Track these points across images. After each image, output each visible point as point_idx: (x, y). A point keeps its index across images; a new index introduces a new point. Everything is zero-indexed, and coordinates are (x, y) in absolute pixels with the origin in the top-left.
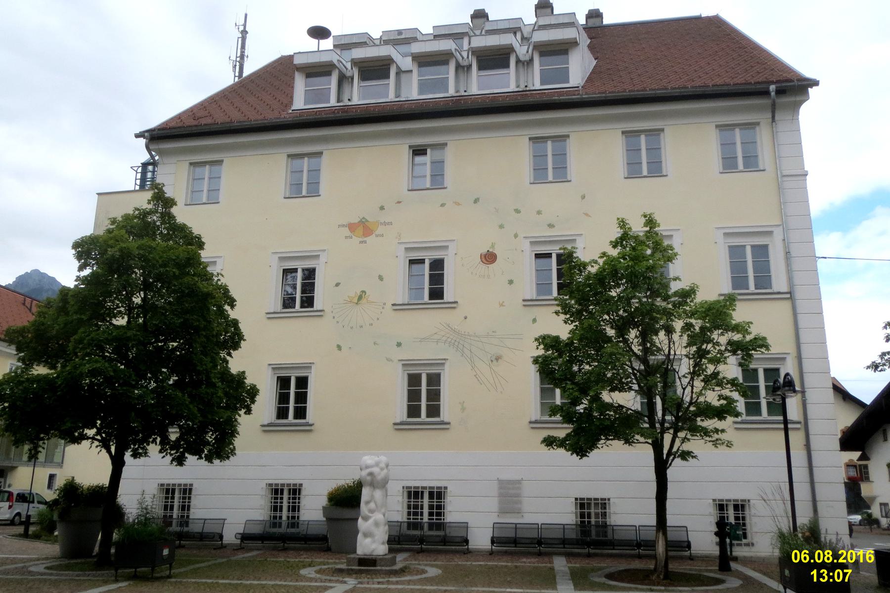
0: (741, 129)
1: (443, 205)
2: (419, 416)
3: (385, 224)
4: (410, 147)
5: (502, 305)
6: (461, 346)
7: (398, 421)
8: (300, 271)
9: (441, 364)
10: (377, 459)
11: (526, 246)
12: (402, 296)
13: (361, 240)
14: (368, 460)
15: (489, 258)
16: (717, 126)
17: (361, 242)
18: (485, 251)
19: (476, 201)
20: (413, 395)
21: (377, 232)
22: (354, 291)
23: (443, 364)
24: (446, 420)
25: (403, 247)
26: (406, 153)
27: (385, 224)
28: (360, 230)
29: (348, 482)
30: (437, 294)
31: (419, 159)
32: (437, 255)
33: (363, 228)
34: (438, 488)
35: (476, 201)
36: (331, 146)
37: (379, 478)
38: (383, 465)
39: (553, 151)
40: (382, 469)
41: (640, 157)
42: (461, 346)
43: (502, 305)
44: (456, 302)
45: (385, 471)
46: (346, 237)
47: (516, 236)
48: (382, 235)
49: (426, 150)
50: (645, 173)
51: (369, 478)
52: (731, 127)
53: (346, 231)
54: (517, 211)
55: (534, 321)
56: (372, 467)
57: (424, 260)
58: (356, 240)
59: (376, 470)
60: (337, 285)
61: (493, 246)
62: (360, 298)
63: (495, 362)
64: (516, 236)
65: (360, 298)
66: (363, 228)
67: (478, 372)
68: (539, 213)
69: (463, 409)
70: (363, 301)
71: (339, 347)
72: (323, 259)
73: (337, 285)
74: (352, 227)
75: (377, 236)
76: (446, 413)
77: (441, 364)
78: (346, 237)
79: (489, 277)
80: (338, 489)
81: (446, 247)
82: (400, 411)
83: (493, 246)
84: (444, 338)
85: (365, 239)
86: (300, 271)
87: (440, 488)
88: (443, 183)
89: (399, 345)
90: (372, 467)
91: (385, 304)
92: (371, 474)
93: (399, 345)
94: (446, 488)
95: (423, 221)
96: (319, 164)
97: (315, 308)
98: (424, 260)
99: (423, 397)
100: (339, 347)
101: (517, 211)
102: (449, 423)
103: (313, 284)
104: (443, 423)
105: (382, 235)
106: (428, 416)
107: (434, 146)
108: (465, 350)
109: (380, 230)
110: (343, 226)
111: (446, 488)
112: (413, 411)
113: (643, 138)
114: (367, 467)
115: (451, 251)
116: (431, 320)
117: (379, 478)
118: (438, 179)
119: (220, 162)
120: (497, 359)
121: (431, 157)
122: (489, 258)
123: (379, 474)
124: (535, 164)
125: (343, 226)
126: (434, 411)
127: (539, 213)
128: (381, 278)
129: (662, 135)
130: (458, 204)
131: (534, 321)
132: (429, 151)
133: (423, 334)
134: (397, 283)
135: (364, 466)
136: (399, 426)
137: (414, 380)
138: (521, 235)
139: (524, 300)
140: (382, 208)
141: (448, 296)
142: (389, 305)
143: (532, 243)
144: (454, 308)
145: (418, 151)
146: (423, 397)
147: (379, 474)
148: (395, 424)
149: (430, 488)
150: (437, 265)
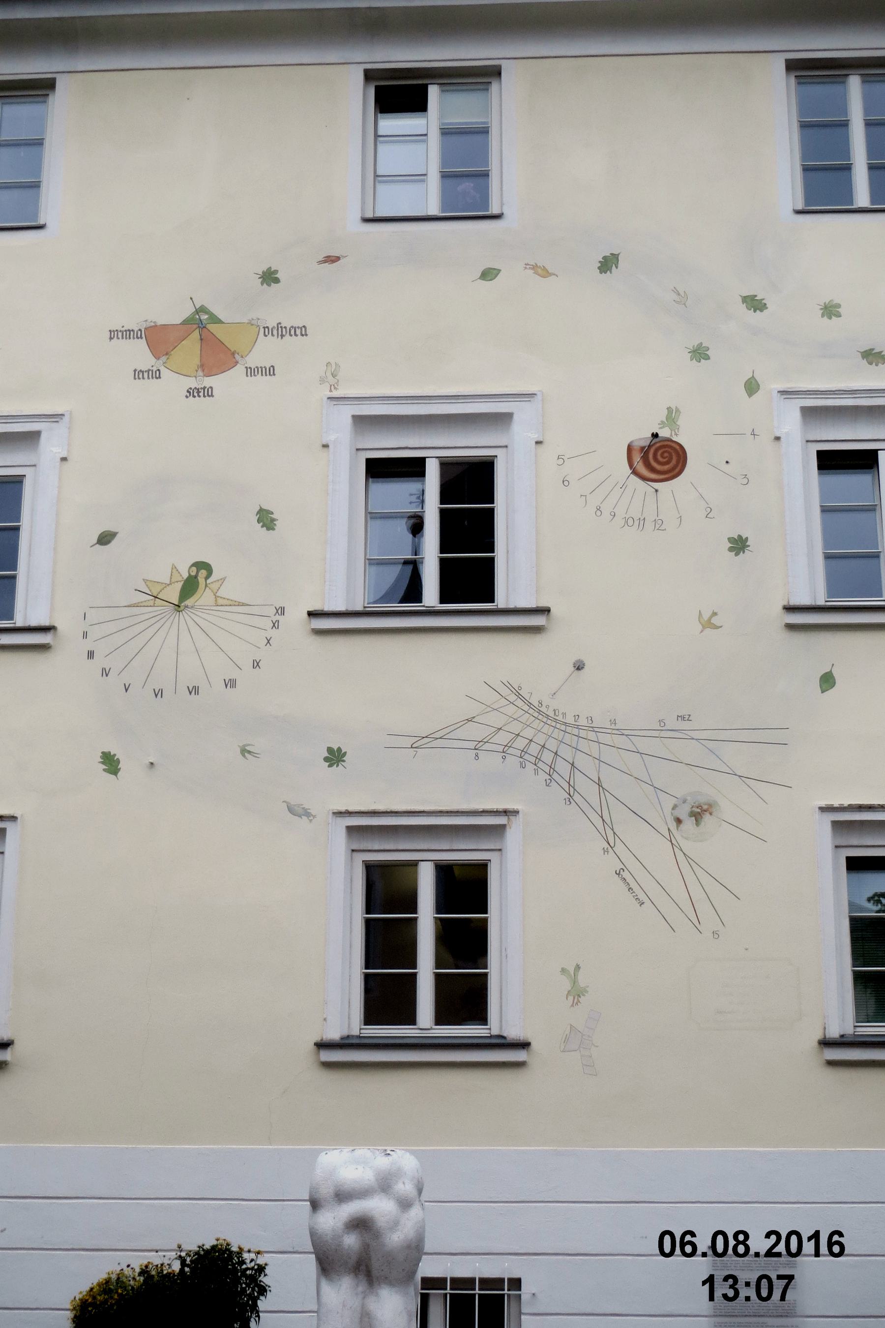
0: (866, 80)
1: (488, 274)
2: (410, 1018)
3: (281, 331)
4: (369, 76)
5: (709, 624)
6: (563, 768)
7: (334, 1035)
8: (433, 471)
9: (492, 828)
10: (382, 1162)
11: (790, 421)
12: (344, 582)
13: (192, 383)
14: (347, 1164)
15: (660, 459)
16: (792, 66)
17: (192, 393)
18: (642, 436)
19: (608, 264)
20: (387, 943)
21: (254, 359)
22: (169, 563)
23: (499, 830)
24: (513, 1033)
25: (348, 412)
26: (354, 96)
27: (281, 331)
28: (190, 349)
29: (156, 1259)
30: (470, 579)
31: (393, 124)
32: (467, 445)
33: (199, 343)
34: (486, 1283)
35: (608, 264)
36: (82, 63)
37: (396, 1239)
38: (405, 1187)
39: (867, 110)
40: (405, 1204)
41: (845, 149)
42: (563, 768)
43: (709, 624)
44: (545, 611)
45: (415, 1212)
46: (138, 374)
47: (752, 387)
48: (271, 371)
49: (423, 92)
50: (862, 197)
51: (351, 1241)
52: (832, 69)
53: (140, 354)
54: (755, 304)
55: (827, 681)
56: (363, 1193)
57: (422, 461)
58: (174, 383)
59: (380, 1207)
60: (105, 539)
61: (672, 417)
62: (190, 587)
63: (689, 824)
64: (752, 387)
65: (190, 587)
66: (199, 343)
67: (631, 863)
68: (830, 311)
69: (577, 994)
70: (203, 598)
71: (110, 763)
72: (52, 445)
73: (105, 539)
74: (159, 339)
75: (251, 372)
76: (506, 1013)
77: (492, 828)
78: (138, 374)
79: (659, 524)
80: (106, 1287)
81: (502, 420)
82: (338, 998)
83: (672, 417)
84: (503, 738)
85: (208, 382)
86: (433, 471)
87: (497, 1283)
88: (36, 215)
89: (335, 757)
90: (363, 1193)
91: (281, 611)
92: (361, 1224)
93: (335, 757)
94: (516, 1283)
95: (425, 333)
96: (41, 122)
97: (502, 600)
98: (422, 461)
99: (426, 947)
100: (110, 763)
101: (755, 304)
102: (524, 1045)
103: (488, 518)
104: (501, 1043)
105: (271, 371)
106: (441, 1018)
107: (458, 78)
108: (580, 782)
109: (264, 351)
110: (128, 334)
111: (516, 1283)
112: (387, 999)
113: (854, 83)
114: (342, 1196)
115: (522, 433)
116: (445, 671)
117: (396, 1239)
118: (468, 193)
119: (42, 88)
120: (698, 814)
121: (442, 116)
122: (660, 459)
123: (395, 1224)
124: (807, 151)
125: (128, 334)
126: (465, 999)
127: (830, 311)
128: (266, 519)
129: (494, 87)
130: (544, 272)
131: (827, 681)
132: (433, 92)
133: (420, 722)
134: (332, 538)
135: (326, 1191)
136: (336, 1054)
137: (386, 891)
138: (772, 385)
139: (790, 609)
140: (269, 277)
141: (510, 588)
142: (297, 614)
143: (810, 414)
144: (537, 630)
145: (398, 94)
146: (426, 947)
147: (395, 1224)
148: (322, 1045)
149: (457, 1282)
150: (470, 483)
